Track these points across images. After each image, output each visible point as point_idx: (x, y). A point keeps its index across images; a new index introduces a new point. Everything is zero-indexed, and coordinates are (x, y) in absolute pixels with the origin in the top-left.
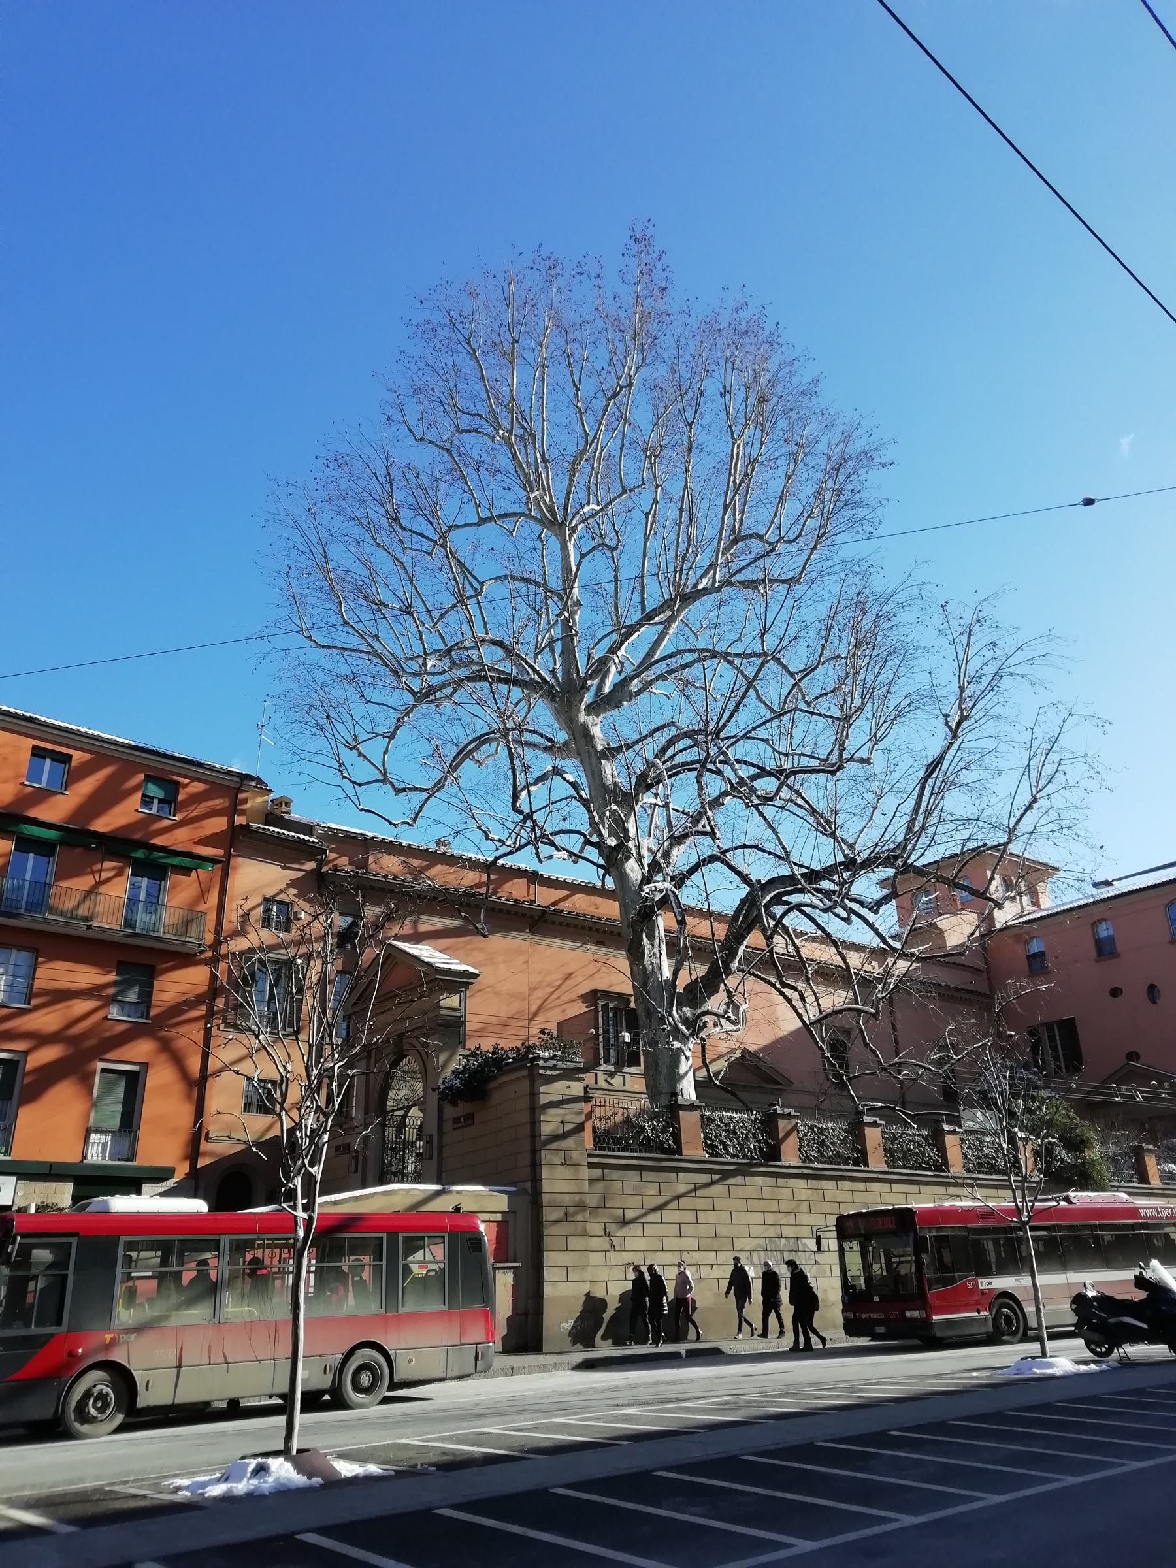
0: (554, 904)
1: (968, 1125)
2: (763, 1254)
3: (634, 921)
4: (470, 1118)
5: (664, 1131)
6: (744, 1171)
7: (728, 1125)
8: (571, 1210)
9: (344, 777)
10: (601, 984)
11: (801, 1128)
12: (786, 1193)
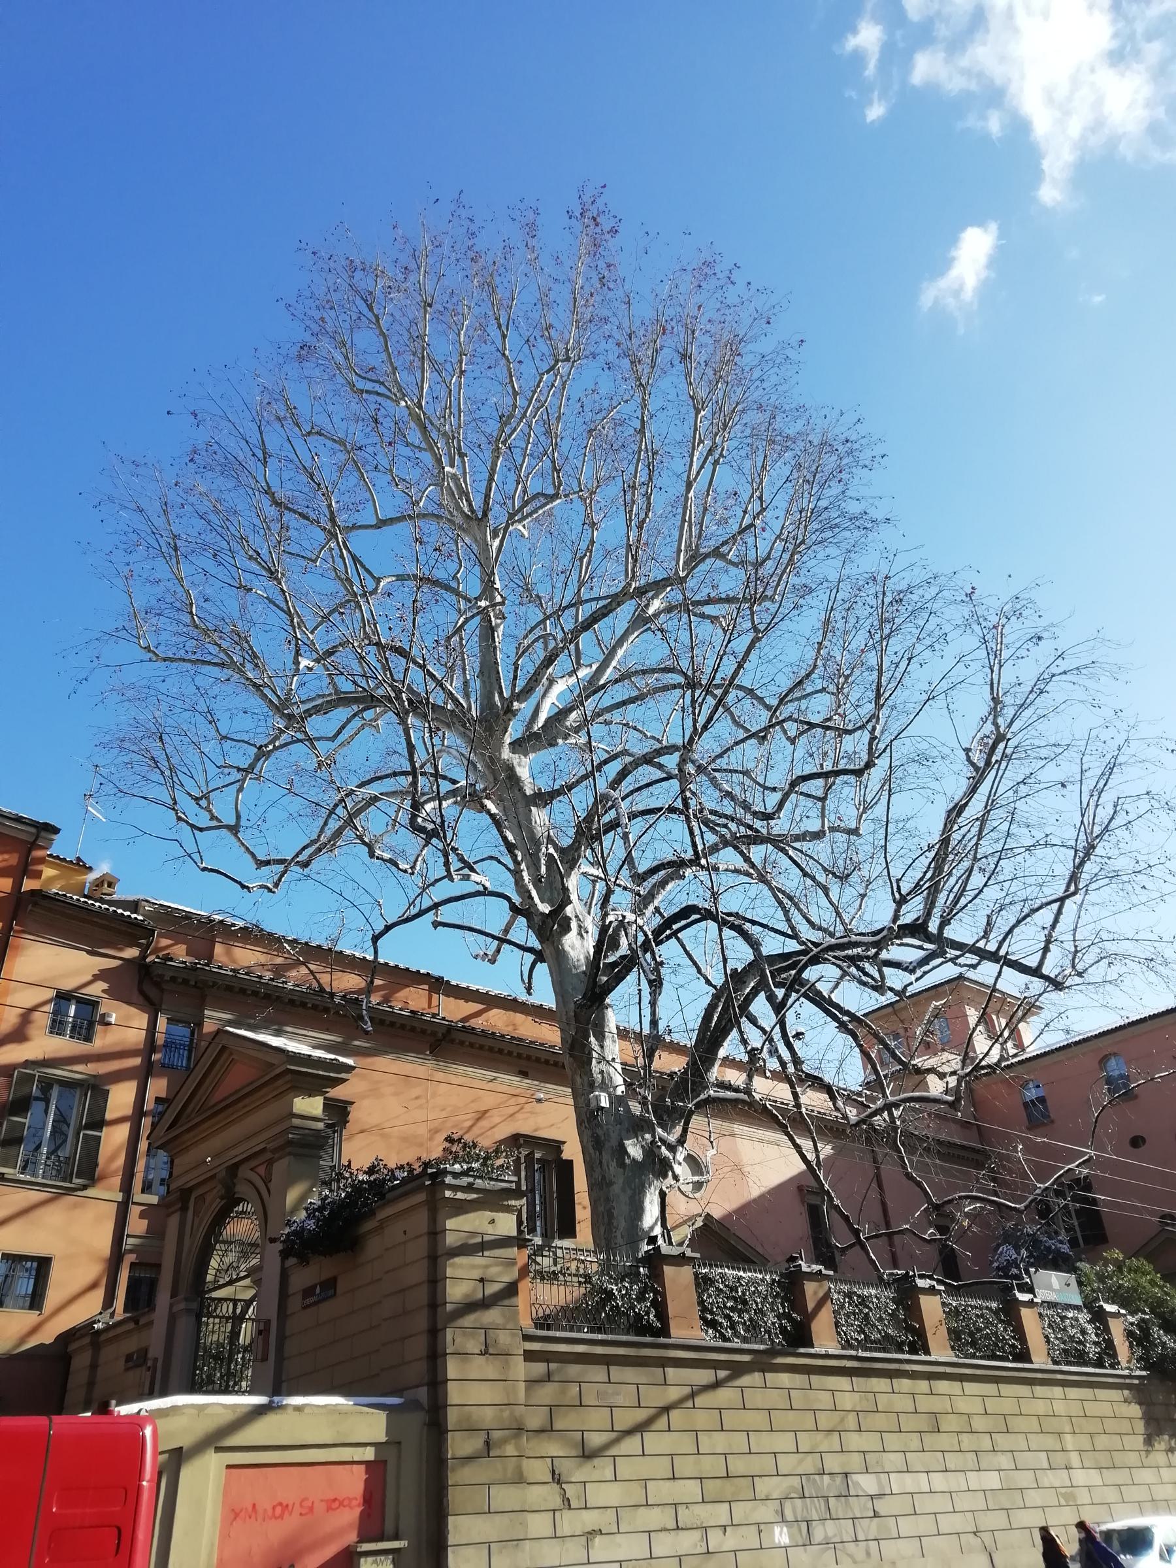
0: (464, 1020)
1: (1041, 1295)
2: (799, 1502)
3: (579, 1006)
4: (329, 1286)
5: (641, 1298)
6: (763, 1363)
7: (733, 1289)
8: (496, 1435)
9: (179, 819)
10: (525, 1126)
11: (836, 1296)
12: (824, 1399)
